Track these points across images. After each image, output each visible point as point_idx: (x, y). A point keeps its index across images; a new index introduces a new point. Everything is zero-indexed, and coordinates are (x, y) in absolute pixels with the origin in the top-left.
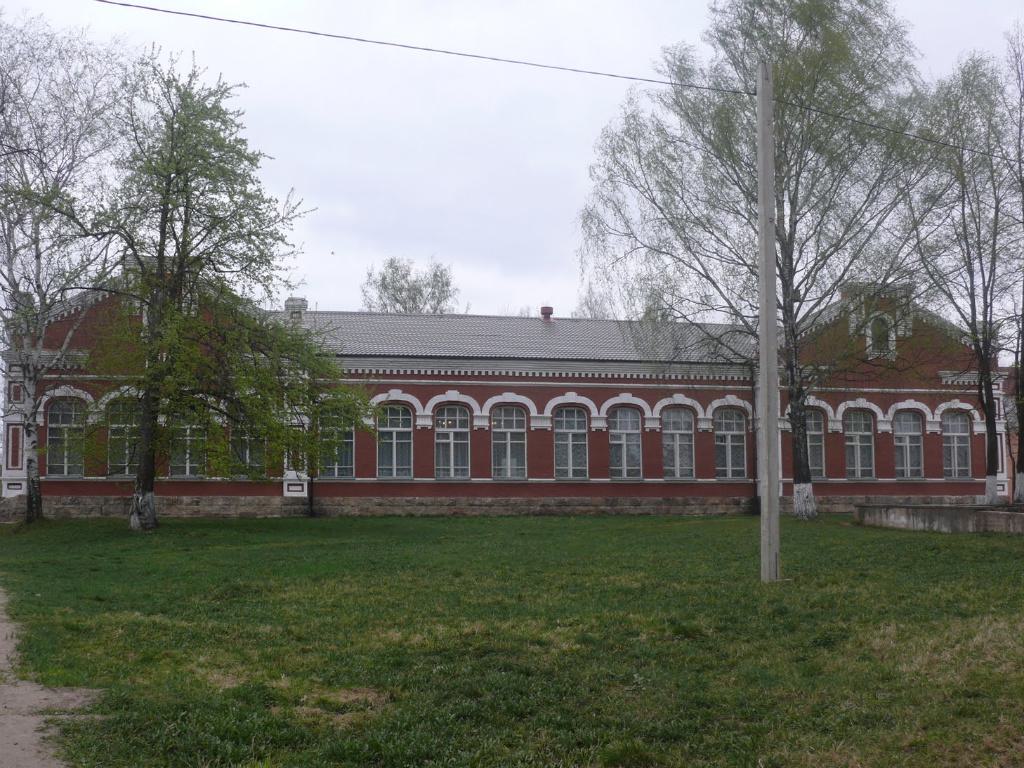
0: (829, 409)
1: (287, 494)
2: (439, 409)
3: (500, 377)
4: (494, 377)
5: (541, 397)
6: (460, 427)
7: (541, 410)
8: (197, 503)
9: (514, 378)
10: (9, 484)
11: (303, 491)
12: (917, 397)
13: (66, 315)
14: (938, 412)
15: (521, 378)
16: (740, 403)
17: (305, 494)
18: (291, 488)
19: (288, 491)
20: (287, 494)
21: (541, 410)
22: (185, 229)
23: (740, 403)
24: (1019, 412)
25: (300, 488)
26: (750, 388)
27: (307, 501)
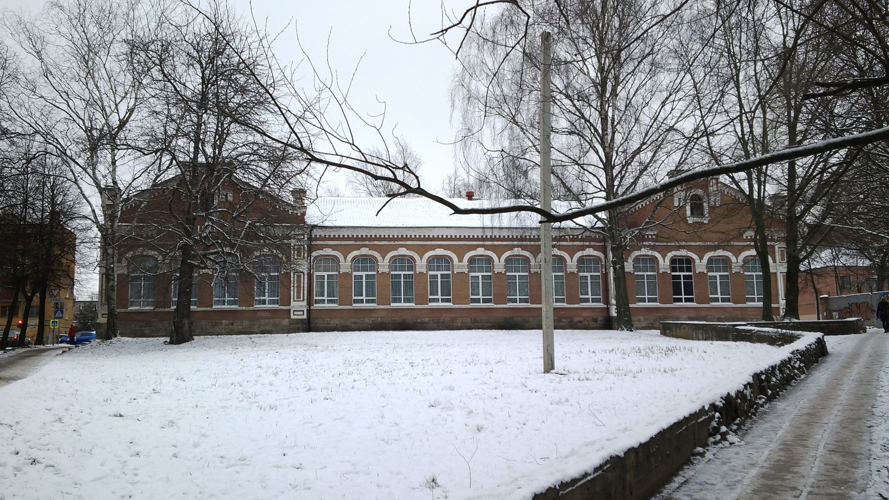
0: (379, 258)
1: (292, 317)
2: (581, 260)
3: (433, 239)
4: (429, 239)
5: (460, 251)
6: (680, 275)
7: (460, 260)
8: (232, 324)
9: (442, 239)
10: (103, 314)
11: (303, 315)
12: (689, 248)
13: (134, 205)
14: (575, 258)
15: (447, 239)
16: (596, 253)
17: (305, 317)
18: (296, 313)
19: (294, 315)
20: (292, 317)
21: (460, 260)
22: (813, 38)
23: (596, 253)
24: (74, 255)
25: (301, 313)
26: (602, 244)
27: (306, 322)
